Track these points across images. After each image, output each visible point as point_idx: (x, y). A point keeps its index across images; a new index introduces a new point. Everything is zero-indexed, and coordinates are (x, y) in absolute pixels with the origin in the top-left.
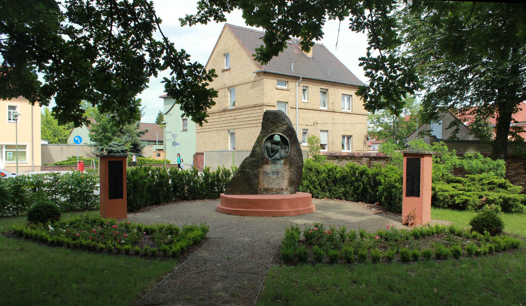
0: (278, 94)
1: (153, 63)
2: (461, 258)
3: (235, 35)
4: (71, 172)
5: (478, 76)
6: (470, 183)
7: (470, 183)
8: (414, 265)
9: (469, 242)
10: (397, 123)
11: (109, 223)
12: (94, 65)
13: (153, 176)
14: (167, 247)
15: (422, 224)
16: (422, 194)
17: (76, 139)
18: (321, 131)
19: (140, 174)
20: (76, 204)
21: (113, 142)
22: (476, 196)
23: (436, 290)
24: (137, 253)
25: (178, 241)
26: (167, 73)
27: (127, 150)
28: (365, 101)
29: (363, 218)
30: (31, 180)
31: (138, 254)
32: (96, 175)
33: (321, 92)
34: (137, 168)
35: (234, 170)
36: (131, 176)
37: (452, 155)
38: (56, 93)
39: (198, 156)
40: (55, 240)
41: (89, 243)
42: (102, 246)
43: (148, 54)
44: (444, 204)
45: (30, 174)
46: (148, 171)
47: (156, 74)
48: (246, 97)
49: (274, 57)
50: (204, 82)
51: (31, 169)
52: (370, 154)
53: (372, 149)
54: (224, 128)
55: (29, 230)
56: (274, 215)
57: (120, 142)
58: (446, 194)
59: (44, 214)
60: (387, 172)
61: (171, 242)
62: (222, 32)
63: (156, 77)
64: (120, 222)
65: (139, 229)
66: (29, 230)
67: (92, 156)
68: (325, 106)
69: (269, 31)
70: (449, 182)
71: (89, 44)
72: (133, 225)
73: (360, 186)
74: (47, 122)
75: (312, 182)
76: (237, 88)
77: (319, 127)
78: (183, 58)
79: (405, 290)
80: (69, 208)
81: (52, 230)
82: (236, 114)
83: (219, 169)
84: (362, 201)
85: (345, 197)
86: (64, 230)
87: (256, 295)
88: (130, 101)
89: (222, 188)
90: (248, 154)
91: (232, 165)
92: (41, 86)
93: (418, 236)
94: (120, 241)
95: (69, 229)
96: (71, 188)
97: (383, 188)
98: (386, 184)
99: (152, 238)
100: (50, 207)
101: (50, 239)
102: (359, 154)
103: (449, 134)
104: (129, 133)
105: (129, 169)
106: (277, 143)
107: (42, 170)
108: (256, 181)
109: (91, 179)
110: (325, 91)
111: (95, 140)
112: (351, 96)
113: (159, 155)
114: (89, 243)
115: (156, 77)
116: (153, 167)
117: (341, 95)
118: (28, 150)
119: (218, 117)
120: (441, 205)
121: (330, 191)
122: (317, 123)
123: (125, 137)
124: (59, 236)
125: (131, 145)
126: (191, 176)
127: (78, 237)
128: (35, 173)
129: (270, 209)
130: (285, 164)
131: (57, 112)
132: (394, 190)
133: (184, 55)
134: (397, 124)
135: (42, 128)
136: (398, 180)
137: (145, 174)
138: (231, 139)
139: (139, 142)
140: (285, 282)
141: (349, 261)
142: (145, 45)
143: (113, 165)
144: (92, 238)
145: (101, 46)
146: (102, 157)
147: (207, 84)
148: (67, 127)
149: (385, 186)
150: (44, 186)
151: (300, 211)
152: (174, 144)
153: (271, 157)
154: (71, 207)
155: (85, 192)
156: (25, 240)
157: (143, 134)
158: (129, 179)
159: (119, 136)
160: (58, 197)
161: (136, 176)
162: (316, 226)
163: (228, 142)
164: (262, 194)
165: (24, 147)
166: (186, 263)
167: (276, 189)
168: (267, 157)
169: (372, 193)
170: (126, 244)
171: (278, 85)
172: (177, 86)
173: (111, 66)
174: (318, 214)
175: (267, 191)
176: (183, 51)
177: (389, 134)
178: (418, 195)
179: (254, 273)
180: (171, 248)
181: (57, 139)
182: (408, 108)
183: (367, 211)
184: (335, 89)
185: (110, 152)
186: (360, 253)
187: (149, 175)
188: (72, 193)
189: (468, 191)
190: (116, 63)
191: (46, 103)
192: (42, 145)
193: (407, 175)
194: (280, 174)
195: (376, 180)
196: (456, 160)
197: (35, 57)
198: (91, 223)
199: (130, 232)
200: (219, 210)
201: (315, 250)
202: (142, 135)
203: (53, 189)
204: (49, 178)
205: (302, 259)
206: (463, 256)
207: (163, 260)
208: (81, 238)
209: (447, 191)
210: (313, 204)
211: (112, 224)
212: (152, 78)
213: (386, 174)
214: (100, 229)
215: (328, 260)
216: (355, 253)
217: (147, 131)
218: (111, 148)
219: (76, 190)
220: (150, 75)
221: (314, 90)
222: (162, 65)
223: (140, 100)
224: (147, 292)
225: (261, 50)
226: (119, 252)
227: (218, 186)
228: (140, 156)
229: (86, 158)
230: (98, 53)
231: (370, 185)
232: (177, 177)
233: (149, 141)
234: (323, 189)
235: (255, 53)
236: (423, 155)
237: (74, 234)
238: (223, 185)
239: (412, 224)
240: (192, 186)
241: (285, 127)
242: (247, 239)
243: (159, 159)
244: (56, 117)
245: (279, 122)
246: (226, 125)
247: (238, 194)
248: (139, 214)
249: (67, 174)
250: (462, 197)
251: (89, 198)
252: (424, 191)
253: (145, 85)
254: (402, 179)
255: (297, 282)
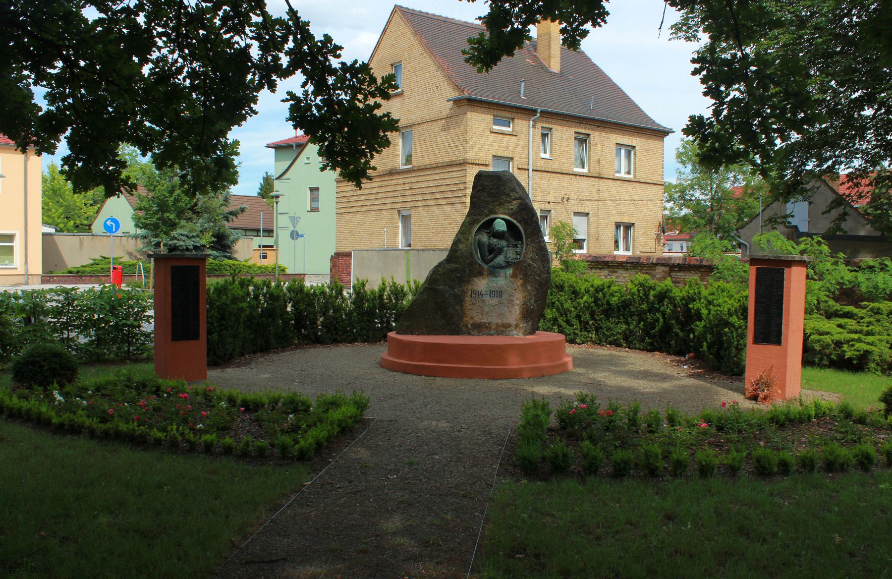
0: (495, 142)
1: (267, 63)
2: (876, 471)
3: (414, 27)
4: (98, 287)
5: (883, 111)
6: (871, 319)
7: (871, 319)
8: (786, 483)
9: (882, 436)
10: (719, 200)
11: (173, 388)
12: (146, 70)
13: (256, 297)
14: (287, 439)
15: (784, 398)
16: (787, 340)
17: (109, 223)
18: (576, 214)
19: (233, 292)
20: (108, 350)
21: (179, 231)
22: (884, 343)
23: (838, 538)
24: (228, 451)
25: (309, 426)
26: (295, 83)
27: (204, 246)
28: (701, 146)
29: (666, 385)
30: (21, 301)
31: (231, 453)
32: (147, 294)
33: (576, 139)
34: (226, 281)
35: (413, 286)
36: (215, 297)
37: (836, 263)
38: (69, 128)
39: (340, 260)
40: (67, 422)
41: (133, 430)
42: (159, 435)
43: (256, 44)
44: (821, 359)
45: (19, 290)
46: (248, 286)
47: (272, 87)
48: (430, 146)
49: (505, 58)
50: (371, 101)
51: (22, 280)
52: (670, 258)
53: (666, 250)
54: (389, 206)
55: (15, 402)
56: (493, 375)
57: (191, 231)
58: (827, 339)
59: (46, 368)
60: (713, 294)
61: (295, 429)
62: (389, 22)
63: (273, 91)
64: (195, 386)
65: (231, 401)
66: (15, 399)
67: (139, 256)
68: (583, 167)
69: (497, 5)
70: (829, 315)
71: (137, 25)
72: (218, 392)
73: (658, 320)
74: (54, 191)
75: (564, 313)
76: (416, 131)
77: (573, 206)
78: (326, 53)
79: (774, 535)
80: (93, 357)
81: (59, 401)
82: (413, 180)
83: (383, 284)
84: (660, 350)
85: (628, 341)
86: (85, 402)
87: (474, 544)
88: (216, 144)
89: (388, 322)
90: (444, 256)
91: (411, 277)
92: (40, 114)
93: (786, 422)
94: (195, 424)
95: (93, 400)
96: (99, 319)
97: (705, 327)
98: (711, 317)
99: (258, 421)
100: (57, 355)
101: (55, 420)
102: (648, 258)
103: (825, 225)
104: (209, 213)
105: (211, 282)
106: (499, 235)
107: (43, 282)
108: (458, 308)
109: (137, 300)
110: (584, 137)
111: (145, 226)
112: (634, 147)
113: (265, 257)
114: (133, 430)
115: (273, 91)
116: (258, 280)
117: (614, 147)
118: (18, 244)
119: (379, 184)
120: (816, 360)
121: (597, 330)
122: (568, 199)
123: (201, 221)
124: (74, 413)
125: (213, 236)
126: (330, 296)
127: (112, 416)
128: (28, 288)
129: (487, 364)
130: (514, 276)
131: (72, 166)
132: (726, 330)
133: (329, 47)
134: (719, 201)
135: (45, 203)
136: (736, 311)
137: (241, 293)
138: (404, 227)
139: (228, 231)
140: (530, 517)
141: (652, 472)
142: (250, 25)
143: (180, 274)
144: (138, 419)
145: (160, 29)
146: (158, 259)
147: (378, 106)
148: (91, 202)
149: (710, 321)
150: (46, 313)
151: (539, 369)
152: (295, 235)
153: (487, 263)
154: (98, 355)
155: (125, 325)
156: (6, 420)
157: (236, 215)
158: (211, 303)
159: (189, 219)
160: (73, 335)
161: (224, 297)
162: (583, 401)
163: (397, 233)
164: (469, 334)
165: (10, 238)
166: (326, 472)
167: (497, 325)
168: (480, 262)
169: (681, 334)
170: (207, 432)
171: (495, 124)
172: (314, 108)
173: (180, 71)
174: (579, 374)
175: (480, 328)
176: (328, 39)
177: (702, 222)
178: (778, 342)
179: (465, 496)
180: (296, 442)
181: (72, 223)
182: (739, 172)
183: (673, 371)
184: (603, 134)
185: (173, 249)
186: (675, 456)
187: (248, 294)
188: (99, 329)
189: (868, 333)
190: (191, 64)
191: (51, 150)
192: (44, 235)
193: (757, 301)
194: (505, 296)
195: (689, 310)
196: (845, 274)
197: (29, 56)
198: (137, 388)
199: (213, 406)
200: (385, 365)
201: (585, 450)
202: (234, 218)
203: (64, 319)
204: (56, 298)
205: (558, 468)
206: (876, 465)
207: (280, 465)
208: (116, 419)
209: (827, 333)
210: (568, 356)
211: (177, 391)
212: (264, 94)
213: (710, 298)
214: (154, 401)
215: (610, 469)
216: (665, 457)
217: (242, 210)
218: (175, 242)
219: (107, 322)
220: (260, 86)
221: (564, 135)
222: (284, 66)
223: (236, 143)
224: (252, 534)
225: (480, 42)
226: (192, 447)
227: (381, 317)
228: (230, 258)
229: (126, 259)
230: (155, 44)
231: (677, 319)
232: (303, 299)
233: (246, 230)
234: (585, 326)
235: (467, 47)
236: (790, 263)
237: (104, 411)
238: (391, 315)
239: (765, 398)
240: (331, 317)
241: (514, 205)
242: (443, 425)
243: (265, 263)
244: (69, 175)
245: (505, 194)
246: (394, 200)
247: (423, 334)
248: (229, 370)
249: (91, 290)
250: (857, 345)
251: (133, 337)
252: (790, 335)
253: (251, 109)
254: (745, 310)
255: (554, 515)
